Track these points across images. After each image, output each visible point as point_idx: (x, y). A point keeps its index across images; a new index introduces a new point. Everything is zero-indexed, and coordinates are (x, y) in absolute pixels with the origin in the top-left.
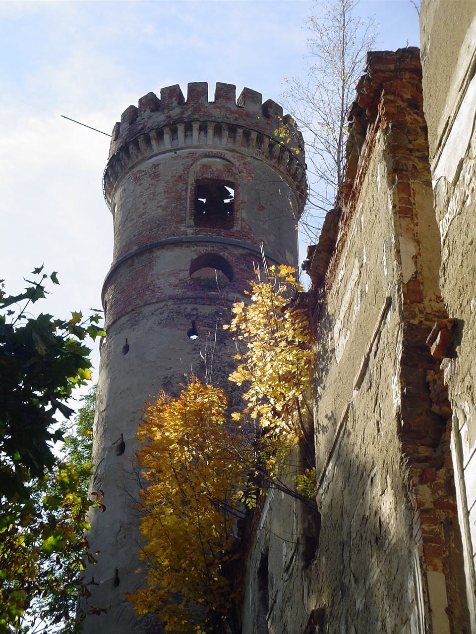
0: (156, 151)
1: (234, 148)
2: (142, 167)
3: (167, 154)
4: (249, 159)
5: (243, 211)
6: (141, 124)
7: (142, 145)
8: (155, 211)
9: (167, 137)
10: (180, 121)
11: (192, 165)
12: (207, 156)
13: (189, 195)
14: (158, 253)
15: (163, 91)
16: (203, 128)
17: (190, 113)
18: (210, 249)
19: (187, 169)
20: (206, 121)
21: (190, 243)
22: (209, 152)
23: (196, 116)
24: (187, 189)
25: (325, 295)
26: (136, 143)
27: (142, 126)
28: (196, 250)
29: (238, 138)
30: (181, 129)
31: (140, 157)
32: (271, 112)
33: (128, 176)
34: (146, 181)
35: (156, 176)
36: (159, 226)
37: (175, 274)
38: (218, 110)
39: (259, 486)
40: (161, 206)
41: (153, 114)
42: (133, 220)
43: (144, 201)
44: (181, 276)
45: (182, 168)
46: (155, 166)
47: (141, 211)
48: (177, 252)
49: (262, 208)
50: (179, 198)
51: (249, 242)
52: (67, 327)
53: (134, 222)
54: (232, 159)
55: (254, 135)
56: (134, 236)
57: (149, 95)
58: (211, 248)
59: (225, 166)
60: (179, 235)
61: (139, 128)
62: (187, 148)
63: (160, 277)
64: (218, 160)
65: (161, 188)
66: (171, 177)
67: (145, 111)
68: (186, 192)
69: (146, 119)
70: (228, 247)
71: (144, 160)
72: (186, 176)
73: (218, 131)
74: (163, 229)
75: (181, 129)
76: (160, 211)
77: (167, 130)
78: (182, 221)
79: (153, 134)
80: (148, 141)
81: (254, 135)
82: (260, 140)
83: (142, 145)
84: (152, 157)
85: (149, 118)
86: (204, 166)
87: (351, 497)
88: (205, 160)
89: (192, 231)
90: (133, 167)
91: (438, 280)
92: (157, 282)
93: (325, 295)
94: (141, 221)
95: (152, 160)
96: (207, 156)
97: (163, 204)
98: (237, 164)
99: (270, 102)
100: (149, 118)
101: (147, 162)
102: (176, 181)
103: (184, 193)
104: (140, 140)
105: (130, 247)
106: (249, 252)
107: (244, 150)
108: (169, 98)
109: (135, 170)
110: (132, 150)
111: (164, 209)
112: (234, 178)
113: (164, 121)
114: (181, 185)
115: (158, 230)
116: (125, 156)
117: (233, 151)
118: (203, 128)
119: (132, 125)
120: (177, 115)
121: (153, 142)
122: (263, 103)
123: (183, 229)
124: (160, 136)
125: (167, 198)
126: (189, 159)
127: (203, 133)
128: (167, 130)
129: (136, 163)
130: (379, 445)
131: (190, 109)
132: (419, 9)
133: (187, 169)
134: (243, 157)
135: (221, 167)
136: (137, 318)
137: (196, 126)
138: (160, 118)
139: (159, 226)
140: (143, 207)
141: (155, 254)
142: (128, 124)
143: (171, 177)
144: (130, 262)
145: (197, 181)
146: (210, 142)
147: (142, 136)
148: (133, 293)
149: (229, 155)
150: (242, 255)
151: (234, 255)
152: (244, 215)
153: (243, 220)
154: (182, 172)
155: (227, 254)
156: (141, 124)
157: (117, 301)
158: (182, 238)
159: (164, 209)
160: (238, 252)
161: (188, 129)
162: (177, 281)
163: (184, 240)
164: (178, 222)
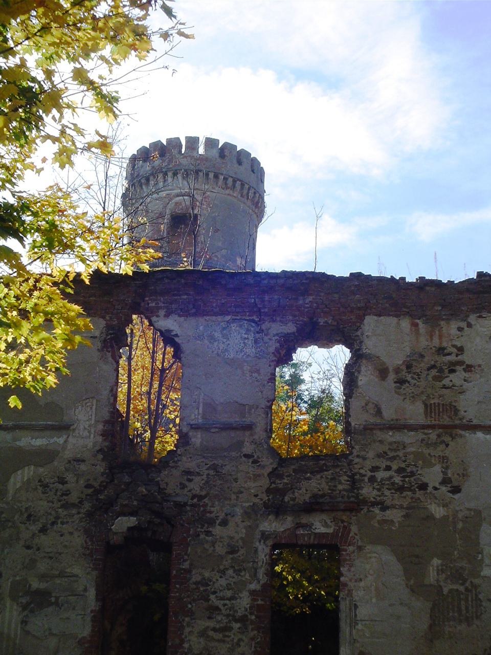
12: (178, 196)
20: (176, 170)
25: (101, 334)
30: (170, 174)
32: (227, 153)
38: (185, 159)
39: (47, 524)
55: (211, 175)
73: (186, 175)
75: (170, 174)
81: (211, 175)
82: (216, 176)
87: (354, 524)
88: (177, 199)
91: (373, 278)
93: (101, 334)
99: (226, 145)
113: (150, 170)
118: (175, 174)
122: (220, 147)
130: (54, 483)
132: (81, 130)
145: (172, 216)
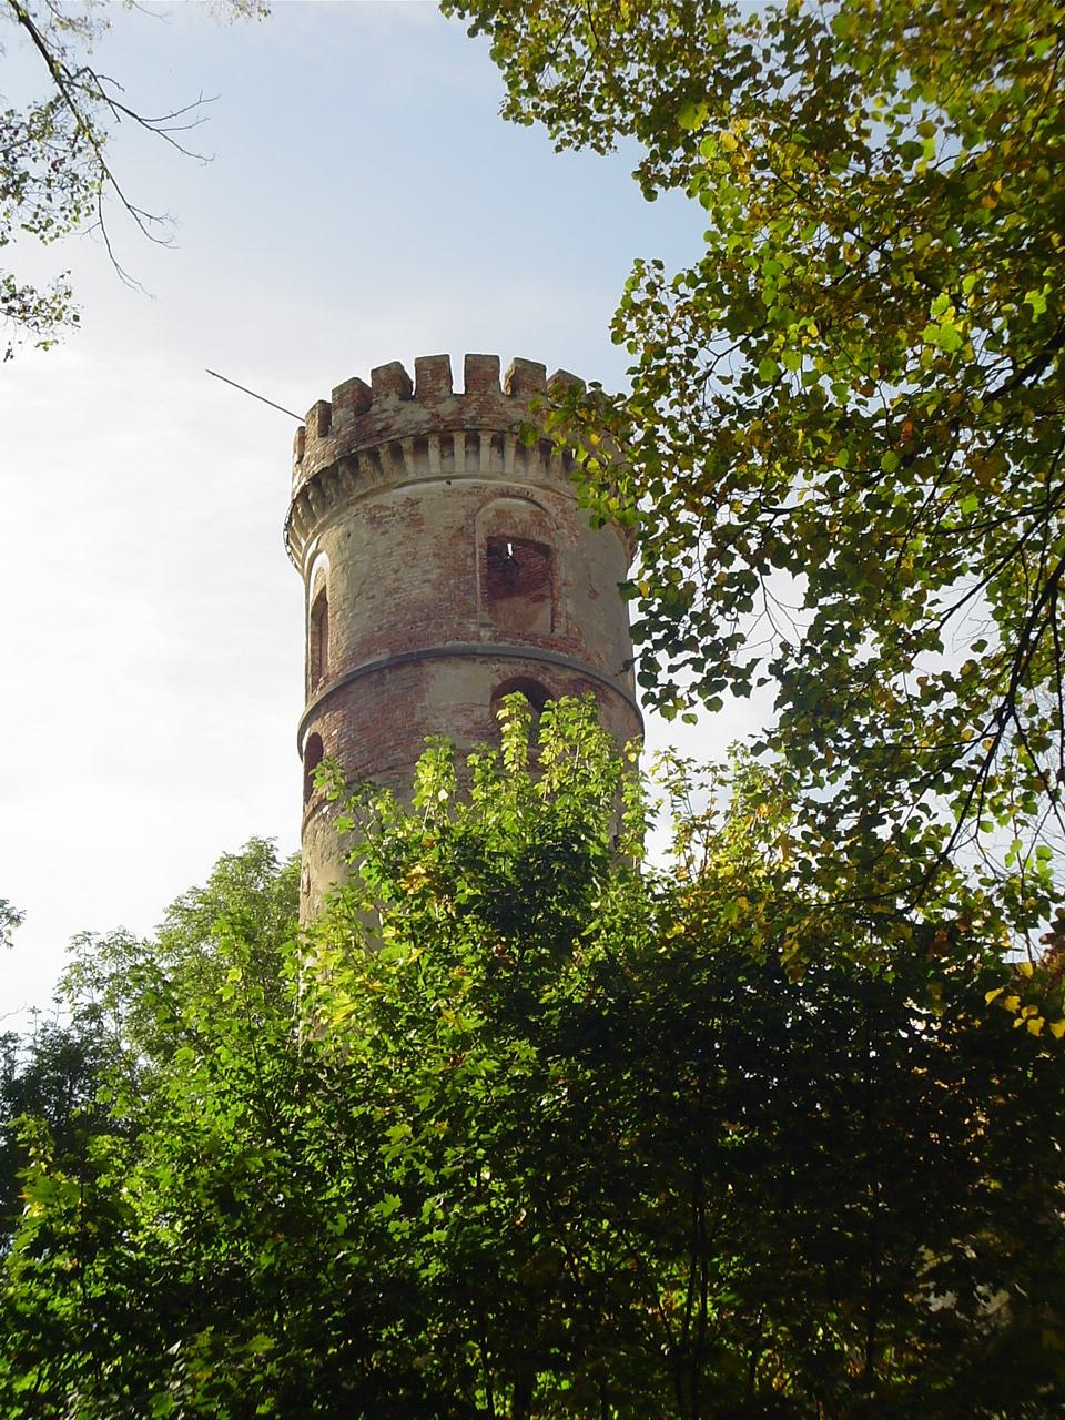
0: (412, 476)
1: (548, 482)
2: (389, 498)
3: (434, 484)
4: (570, 502)
5: (568, 601)
6: (380, 420)
7: (385, 460)
8: (419, 585)
9: (434, 453)
10: (457, 424)
11: (479, 509)
12: (505, 494)
13: (478, 565)
14: (432, 668)
15: (420, 364)
16: (499, 443)
17: (473, 413)
18: (521, 669)
19: (471, 515)
21: (490, 656)
22: (507, 487)
23: (485, 420)
24: (474, 553)
26: (374, 455)
27: (383, 424)
28: (498, 671)
29: (554, 466)
30: (459, 440)
31: (380, 481)
33: (353, 510)
34: (397, 531)
35: (416, 522)
36: (428, 618)
37: (464, 711)
40: (429, 581)
41: (403, 404)
42: (373, 597)
43: (396, 567)
44: (477, 715)
45: (462, 512)
46: (412, 503)
47: (389, 582)
48: (466, 670)
49: (594, 594)
50: (461, 571)
51: (579, 656)
52: (48, 1342)
53: (377, 602)
54: (544, 503)
56: (380, 629)
57: (394, 367)
58: (524, 668)
59: (533, 514)
60: (466, 640)
61: (379, 426)
62: (470, 477)
63: (437, 714)
64: (523, 503)
65: (427, 546)
66: (445, 528)
67: (388, 396)
68: (474, 558)
69: (392, 414)
70: (551, 667)
71: (388, 487)
72: (471, 530)
74: (437, 624)
75: (459, 440)
76: (427, 589)
77: (433, 441)
78: (470, 613)
79: (407, 445)
80: (397, 452)
83: (385, 460)
84: (404, 485)
85: (398, 410)
86: (500, 513)
89: (489, 634)
90: (364, 496)
92: (434, 721)
94: (392, 603)
95: (406, 490)
96: (505, 494)
97: (433, 576)
98: (553, 511)
100: (398, 410)
101: (395, 492)
102: (454, 537)
103: (469, 561)
104: (382, 452)
105: (372, 649)
106: (581, 676)
107: (562, 486)
108: (434, 378)
109: (371, 502)
110: (364, 463)
111: (437, 586)
112: (550, 537)
113: (427, 422)
114: (462, 546)
115: (428, 625)
116: (348, 473)
117: (547, 488)
119: (362, 417)
120: (451, 414)
121: (408, 459)
123: (473, 628)
124: (421, 445)
125: (439, 567)
126: (475, 499)
127: (495, 450)
128: (433, 441)
129: (372, 490)
131: (474, 405)
133: (471, 515)
134: (561, 499)
135: (526, 516)
136: (400, 785)
137: (486, 439)
138: (417, 415)
139: (428, 618)
140: (394, 577)
141: (426, 670)
142: (352, 414)
143: (445, 528)
144: (375, 676)
146: (509, 470)
147: (387, 445)
148: (388, 735)
149: (539, 495)
150: (571, 681)
151: (559, 682)
152: (570, 609)
153: (568, 617)
154: (463, 522)
155: (548, 680)
156: (380, 420)
157: (352, 744)
158: (476, 648)
159: (437, 586)
160: (567, 675)
161: (473, 440)
162: (471, 725)
163: (480, 651)
164: (462, 615)
